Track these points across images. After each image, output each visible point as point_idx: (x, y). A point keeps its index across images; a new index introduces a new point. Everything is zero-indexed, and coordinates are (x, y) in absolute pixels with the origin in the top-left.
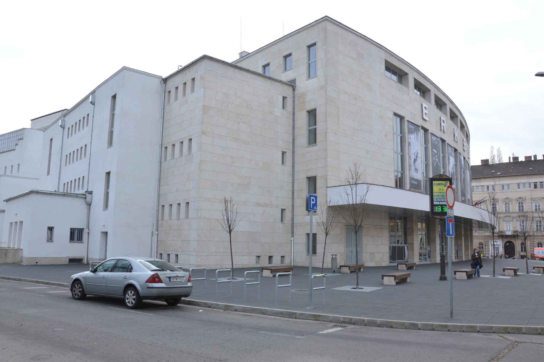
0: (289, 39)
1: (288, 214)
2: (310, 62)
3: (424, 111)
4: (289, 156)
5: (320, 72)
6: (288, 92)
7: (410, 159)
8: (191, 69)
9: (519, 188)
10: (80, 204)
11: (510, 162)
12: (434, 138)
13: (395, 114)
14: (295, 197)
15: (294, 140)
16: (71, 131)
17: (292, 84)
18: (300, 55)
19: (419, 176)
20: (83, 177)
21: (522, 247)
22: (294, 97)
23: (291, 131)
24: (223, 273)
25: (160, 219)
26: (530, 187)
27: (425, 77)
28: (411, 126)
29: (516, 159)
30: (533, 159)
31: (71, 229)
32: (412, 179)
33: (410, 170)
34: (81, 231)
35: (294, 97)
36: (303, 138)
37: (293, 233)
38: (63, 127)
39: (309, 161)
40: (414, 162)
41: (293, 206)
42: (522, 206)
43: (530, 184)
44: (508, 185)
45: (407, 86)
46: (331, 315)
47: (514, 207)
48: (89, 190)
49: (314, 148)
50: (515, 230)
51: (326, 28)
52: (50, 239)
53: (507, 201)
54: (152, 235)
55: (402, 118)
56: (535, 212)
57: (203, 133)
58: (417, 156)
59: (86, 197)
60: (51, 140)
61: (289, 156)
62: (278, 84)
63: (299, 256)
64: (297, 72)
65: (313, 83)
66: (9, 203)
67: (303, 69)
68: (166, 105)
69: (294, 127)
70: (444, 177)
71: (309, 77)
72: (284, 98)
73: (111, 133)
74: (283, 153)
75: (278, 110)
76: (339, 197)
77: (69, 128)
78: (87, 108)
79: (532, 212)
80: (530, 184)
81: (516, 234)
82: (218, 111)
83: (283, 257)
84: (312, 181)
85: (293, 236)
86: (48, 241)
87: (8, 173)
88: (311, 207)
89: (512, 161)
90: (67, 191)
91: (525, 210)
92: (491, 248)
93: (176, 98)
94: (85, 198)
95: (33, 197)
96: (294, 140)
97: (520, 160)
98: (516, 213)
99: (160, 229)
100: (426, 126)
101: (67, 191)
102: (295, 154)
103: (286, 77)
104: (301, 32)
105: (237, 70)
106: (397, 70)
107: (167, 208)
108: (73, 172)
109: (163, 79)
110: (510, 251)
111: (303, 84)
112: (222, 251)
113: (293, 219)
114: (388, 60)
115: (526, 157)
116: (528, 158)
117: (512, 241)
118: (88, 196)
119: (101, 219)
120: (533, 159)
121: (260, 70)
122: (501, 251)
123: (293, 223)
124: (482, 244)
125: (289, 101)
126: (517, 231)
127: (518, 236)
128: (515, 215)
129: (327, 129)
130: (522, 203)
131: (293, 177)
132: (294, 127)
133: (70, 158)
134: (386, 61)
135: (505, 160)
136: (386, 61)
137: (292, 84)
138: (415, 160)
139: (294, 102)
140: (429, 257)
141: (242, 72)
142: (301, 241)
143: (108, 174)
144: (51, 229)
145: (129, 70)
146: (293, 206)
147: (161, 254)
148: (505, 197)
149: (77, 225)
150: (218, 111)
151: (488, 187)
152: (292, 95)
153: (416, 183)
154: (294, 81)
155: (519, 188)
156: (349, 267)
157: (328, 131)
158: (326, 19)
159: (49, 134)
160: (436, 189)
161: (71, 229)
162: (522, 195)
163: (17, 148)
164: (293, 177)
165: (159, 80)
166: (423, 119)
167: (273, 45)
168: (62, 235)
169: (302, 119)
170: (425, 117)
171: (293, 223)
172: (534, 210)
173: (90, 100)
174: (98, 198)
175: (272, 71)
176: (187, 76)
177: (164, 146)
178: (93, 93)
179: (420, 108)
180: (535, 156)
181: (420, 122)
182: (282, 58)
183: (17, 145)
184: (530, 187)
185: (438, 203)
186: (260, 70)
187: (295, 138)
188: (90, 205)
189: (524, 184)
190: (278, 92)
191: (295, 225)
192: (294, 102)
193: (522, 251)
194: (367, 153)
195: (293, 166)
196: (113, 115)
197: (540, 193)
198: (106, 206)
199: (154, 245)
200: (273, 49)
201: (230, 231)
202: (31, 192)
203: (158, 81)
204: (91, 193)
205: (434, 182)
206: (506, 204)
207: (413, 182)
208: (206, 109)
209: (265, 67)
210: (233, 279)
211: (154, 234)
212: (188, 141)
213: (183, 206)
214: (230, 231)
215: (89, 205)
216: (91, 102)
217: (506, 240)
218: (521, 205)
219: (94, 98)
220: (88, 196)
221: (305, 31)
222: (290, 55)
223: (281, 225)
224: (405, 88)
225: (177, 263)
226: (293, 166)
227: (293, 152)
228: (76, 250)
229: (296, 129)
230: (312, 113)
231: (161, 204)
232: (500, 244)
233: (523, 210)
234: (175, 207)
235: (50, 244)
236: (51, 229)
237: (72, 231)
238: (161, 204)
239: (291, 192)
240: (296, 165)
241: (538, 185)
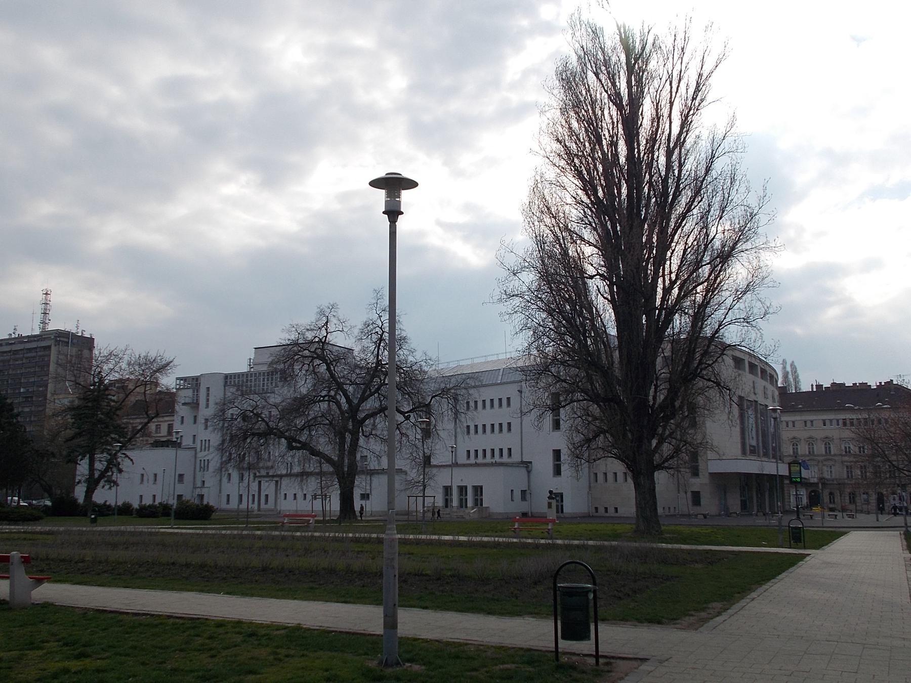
29: (819, 387)
32: (750, 446)
34: (368, 495)
43: (838, 421)
44: (812, 422)
46: (74, 529)
47: (819, 449)
80: (838, 421)
86: (559, 451)
92: (792, 499)
98: (822, 455)
110: (815, 500)
122: (805, 501)
128: (821, 458)
135: (805, 387)
148: (791, 436)
151: (787, 423)
160: (792, 468)
189: (831, 421)
217: (810, 490)
228: (524, 507)
232: (803, 492)
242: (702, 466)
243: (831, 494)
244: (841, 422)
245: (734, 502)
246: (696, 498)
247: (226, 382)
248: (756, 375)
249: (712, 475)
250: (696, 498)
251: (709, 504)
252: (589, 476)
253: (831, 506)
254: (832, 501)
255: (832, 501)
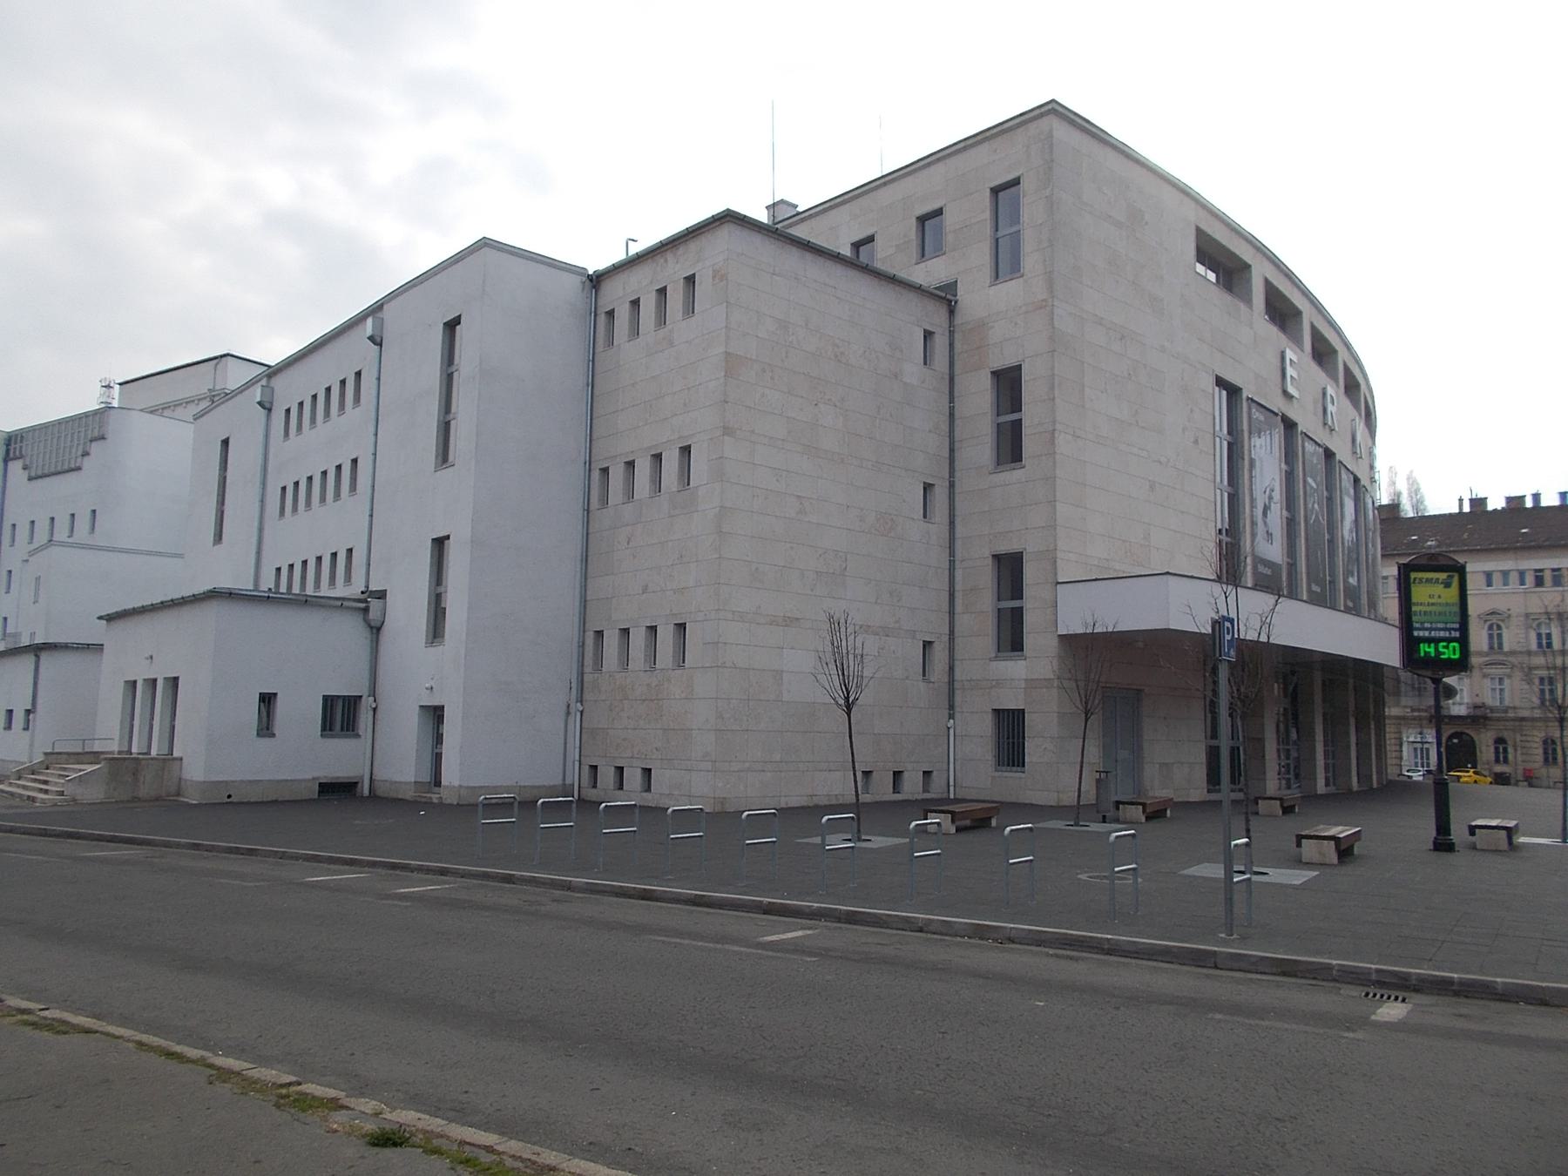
0: (933, 168)
1: (939, 655)
2: (1000, 234)
3: (1290, 371)
4: (940, 494)
5: (1031, 261)
6: (936, 318)
7: (1252, 507)
8: (681, 250)
9: (1489, 584)
10: (350, 630)
11: (1461, 513)
12: (1309, 447)
13: (1220, 382)
14: (959, 608)
15: (952, 450)
16: (297, 418)
17: (946, 297)
18: (968, 215)
19: (1275, 551)
20: (350, 551)
21: (1497, 749)
22: (951, 333)
23: (945, 427)
24: (760, 823)
25: (588, 669)
26: (1522, 583)
27: (1288, 275)
28: (1257, 415)
29: (1478, 503)
30: (1529, 504)
31: (326, 698)
32: (1258, 561)
33: (1253, 535)
34: (352, 703)
35: (951, 333)
36: (979, 446)
37: (951, 707)
38: (267, 407)
39: (999, 509)
40: (1265, 514)
41: (952, 632)
42: (1500, 636)
43: (1522, 574)
45: (1248, 300)
48: (373, 588)
49: (1014, 476)
50: (1478, 701)
51: (1050, 136)
52: (266, 728)
53: (1495, 622)
54: (568, 713)
55: (1233, 391)
56: (1536, 653)
57: (727, 431)
58: (1270, 498)
59: (368, 609)
60: (226, 442)
61: (940, 494)
62: (912, 297)
63: (974, 771)
64: (963, 263)
65: (1010, 290)
66: (119, 626)
67: (980, 255)
68: (599, 348)
69: (952, 415)
70: (1443, 562)
71: (997, 277)
72: (928, 335)
73: (445, 429)
74: (927, 487)
75: (913, 370)
76: (1083, 611)
77: (288, 411)
78: (358, 351)
79: (1529, 653)
80: (1522, 574)
81: (1479, 712)
82: (764, 371)
83: (927, 774)
84: (1010, 569)
85: (951, 716)
87: (61, 534)
88: (1011, 636)
89: (1467, 509)
90: (290, 586)
91: (1506, 648)
93: (635, 331)
94: (366, 610)
95: (213, 610)
96: (952, 450)
97: (1490, 507)
99: (587, 696)
100: (1293, 415)
101: (290, 586)
102: (957, 490)
103: (930, 273)
104: (972, 146)
105: (808, 256)
106: (1227, 260)
107: (611, 641)
108: (302, 538)
109: (590, 278)
111: (978, 297)
112: (778, 757)
113: (951, 669)
114: (1203, 227)
115: (1509, 500)
116: (1515, 503)
117: (1472, 734)
118: (375, 604)
119: (415, 670)
120: (1529, 504)
121: (846, 251)
123: (951, 682)
124: (1553, 742)
125: (941, 342)
126: (1483, 706)
127: (1486, 718)
129: (1054, 422)
130: (1499, 627)
131: (952, 553)
132: (952, 415)
133: (296, 496)
134: (1200, 233)
136: (1200, 233)
137: (946, 297)
138: (1266, 509)
139: (951, 345)
140: (1297, 776)
141: (821, 260)
142: (977, 733)
143: (440, 543)
144: (267, 700)
145: (500, 250)
146: (952, 632)
147: (594, 768)
149: (340, 688)
150: (764, 371)
152: (946, 325)
153: (1269, 573)
154: (951, 287)
155: (1489, 584)
156: (1144, 805)
157: (1058, 426)
158: (1052, 110)
159: (221, 422)
160: (1420, 594)
161: (326, 698)
162: (1500, 604)
163: (87, 463)
164: (952, 553)
165: (579, 279)
166: (1285, 393)
167: (885, 184)
168: (300, 711)
169: (978, 396)
170: (1291, 390)
171: (951, 682)
172: (1534, 647)
173: (369, 332)
174: (406, 611)
175: (883, 255)
176: (672, 271)
177: (596, 467)
178: (376, 309)
179: (1276, 362)
180: (1536, 497)
181: (1278, 404)
182: (914, 221)
183: (86, 454)
184: (1522, 583)
185: (1427, 634)
186: (846, 251)
187: (957, 445)
188: (379, 629)
189: (1505, 574)
190: (910, 319)
191: (957, 685)
192: (951, 345)
193: (1497, 761)
194: (1152, 488)
195: (952, 523)
196: (448, 380)
197: (1550, 597)
198: (436, 630)
199: (574, 742)
200: (885, 195)
201: (849, 708)
202: (213, 595)
203: (576, 281)
204: (381, 595)
205: (1413, 575)
206: (1491, 628)
207: (1261, 569)
208: (732, 364)
209: (857, 246)
210: (859, 840)
211: (572, 710)
212: (677, 452)
213: (666, 636)
214: (849, 708)
215: (376, 630)
216: (371, 338)
218: (1495, 633)
219: (379, 325)
220: (375, 604)
221: (986, 145)
222: (939, 212)
223: (922, 685)
224: (1243, 307)
225: (621, 787)
226: (952, 523)
227: (952, 485)
228: (340, 759)
229: (957, 422)
230: (1008, 383)
231: (593, 626)
233: (1500, 645)
234: (638, 639)
235: (266, 741)
236: (267, 700)
237: (329, 702)
238: (593, 626)
239: (946, 595)
240: (958, 521)
241: (1548, 576)
242: (1032, 619)
243: (1500, 741)
244: (1530, 579)
245: (1176, 762)
246: (1010, 732)
247: (8, 451)
248: (1297, 340)
249: (1070, 642)
250: (1010, 732)
251: (1057, 765)
252: (582, 645)
253: (1499, 769)
254: (1501, 754)
255: (1501, 754)
